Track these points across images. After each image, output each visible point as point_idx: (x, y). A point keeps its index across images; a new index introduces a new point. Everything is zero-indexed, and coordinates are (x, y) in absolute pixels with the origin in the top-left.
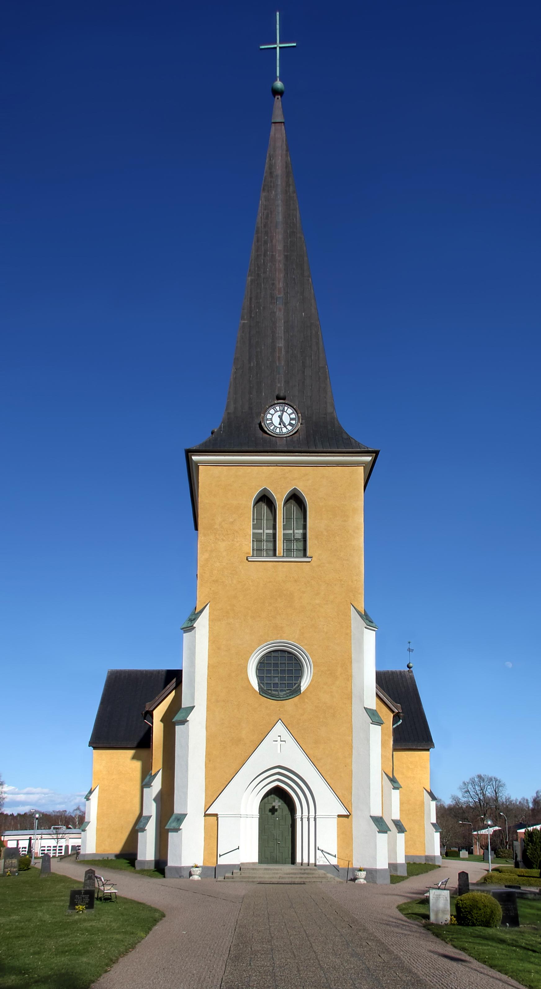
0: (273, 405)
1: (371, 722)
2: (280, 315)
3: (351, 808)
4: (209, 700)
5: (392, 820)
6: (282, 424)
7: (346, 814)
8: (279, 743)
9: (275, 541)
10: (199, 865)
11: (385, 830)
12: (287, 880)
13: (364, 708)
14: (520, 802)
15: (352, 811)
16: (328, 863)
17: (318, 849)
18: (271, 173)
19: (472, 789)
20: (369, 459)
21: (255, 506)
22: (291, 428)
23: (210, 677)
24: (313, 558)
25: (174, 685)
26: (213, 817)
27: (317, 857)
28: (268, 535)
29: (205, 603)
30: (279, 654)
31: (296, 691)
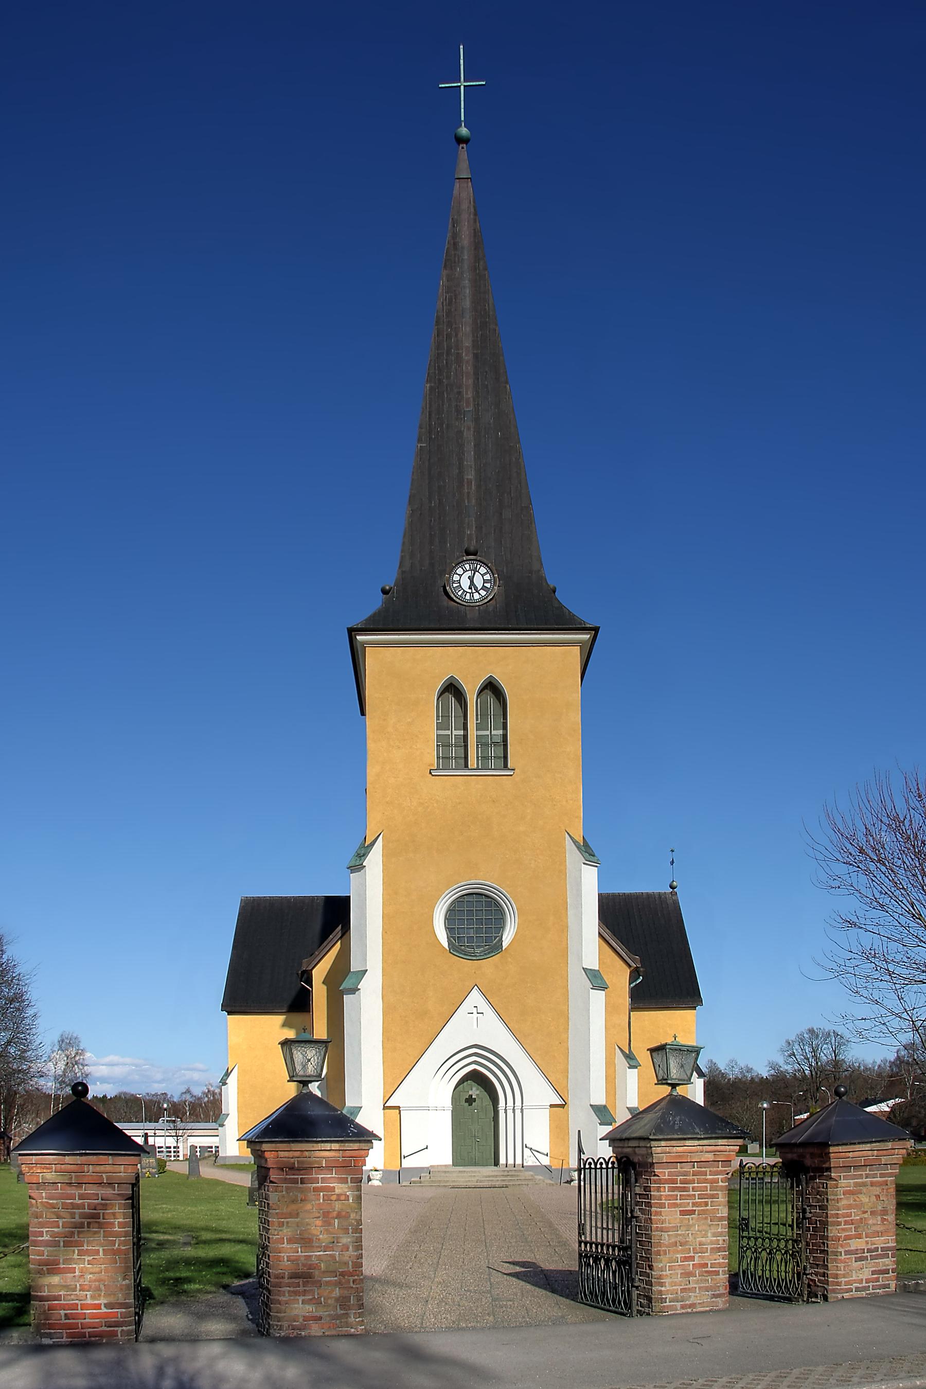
0: (460, 563)
1: (592, 987)
2: (469, 435)
3: (567, 1095)
4: (384, 961)
5: (627, 1108)
6: (473, 588)
7: (561, 1103)
8: (475, 1015)
9: (466, 747)
10: (378, 1169)
11: (609, 1121)
12: (486, 1184)
13: (583, 968)
14: (879, 1066)
15: (568, 1100)
16: (539, 1164)
17: (526, 1147)
18: (455, 244)
19: (800, 1050)
20: (586, 637)
21: (440, 699)
22: (485, 593)
23: (385, 932)
24: (515, 771)
25: (339, 935)
26: (395, 1110)
27: (525, 1157)
28: (457, 738)
29: (377, 832)
30: (475, 898)
31: (496, 948)
